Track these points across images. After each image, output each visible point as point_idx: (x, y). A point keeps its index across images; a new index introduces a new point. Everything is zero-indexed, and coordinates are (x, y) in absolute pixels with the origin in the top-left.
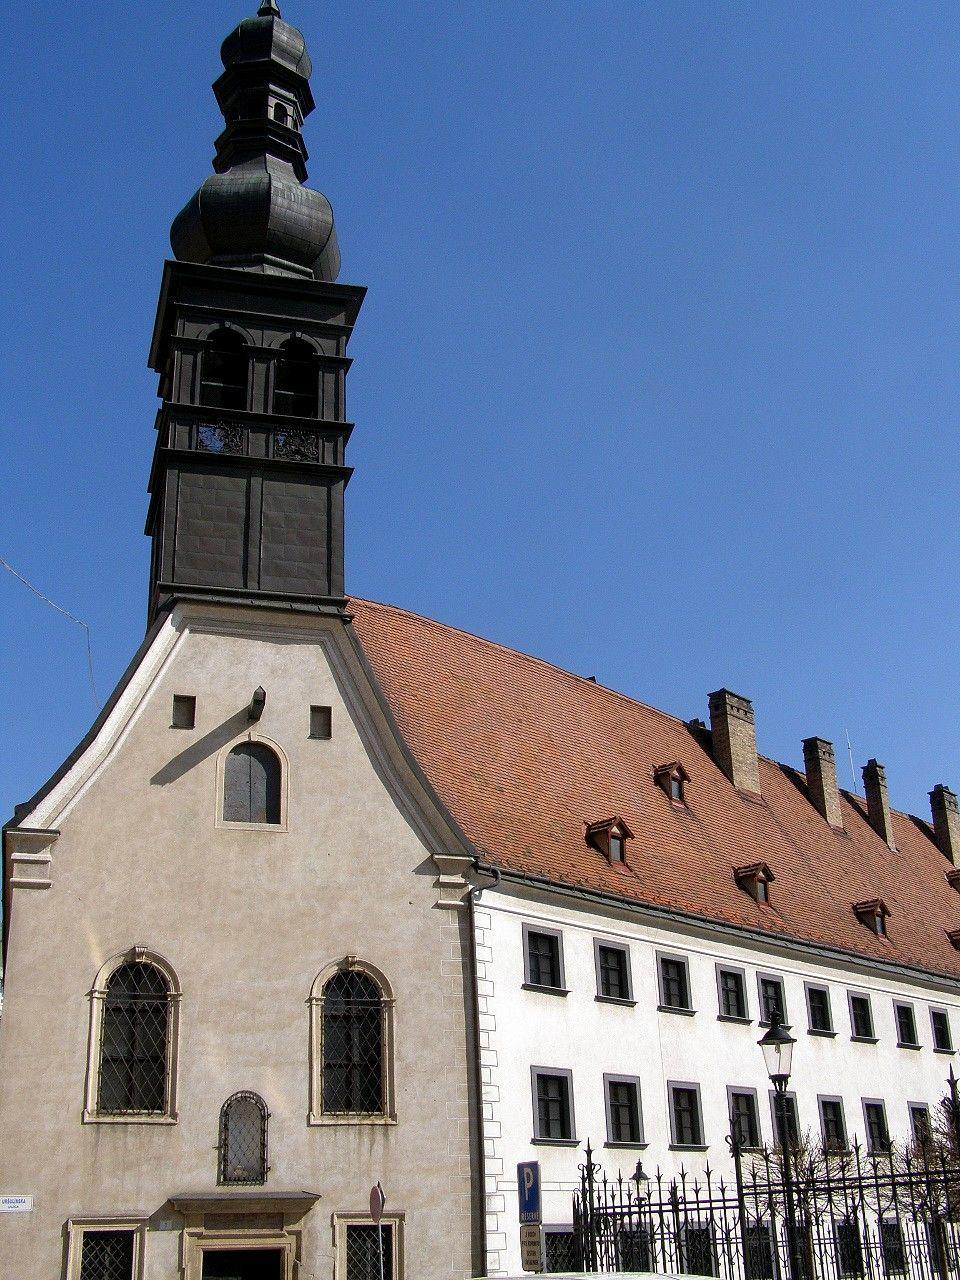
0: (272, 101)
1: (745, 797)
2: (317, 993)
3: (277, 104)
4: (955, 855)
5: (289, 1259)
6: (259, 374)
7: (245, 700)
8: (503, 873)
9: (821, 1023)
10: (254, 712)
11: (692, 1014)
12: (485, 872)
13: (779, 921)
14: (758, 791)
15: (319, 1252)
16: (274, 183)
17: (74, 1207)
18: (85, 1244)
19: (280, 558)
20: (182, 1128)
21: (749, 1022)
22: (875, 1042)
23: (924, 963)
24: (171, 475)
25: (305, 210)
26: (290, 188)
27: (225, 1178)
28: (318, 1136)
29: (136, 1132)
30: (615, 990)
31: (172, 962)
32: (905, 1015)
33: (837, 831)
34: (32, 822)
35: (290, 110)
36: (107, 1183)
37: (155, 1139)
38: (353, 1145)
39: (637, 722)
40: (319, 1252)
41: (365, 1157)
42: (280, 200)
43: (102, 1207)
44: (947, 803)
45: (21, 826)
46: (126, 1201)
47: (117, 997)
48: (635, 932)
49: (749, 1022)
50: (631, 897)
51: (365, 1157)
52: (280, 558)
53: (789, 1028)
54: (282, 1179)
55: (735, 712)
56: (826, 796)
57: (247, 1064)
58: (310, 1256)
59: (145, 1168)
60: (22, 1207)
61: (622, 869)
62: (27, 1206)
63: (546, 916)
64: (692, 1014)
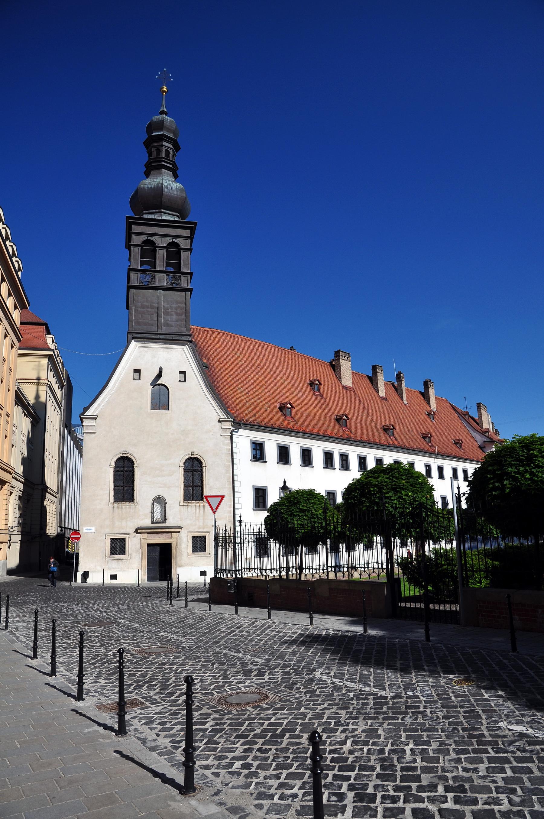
0: (164, 149)
1: (346, 388)
2: (182, 464)
3: (166, 150)
4: (431, 404)
5: (173, 546)
6: (161, 254)
7: (157, 372)
8: (242, 424)
9: (441, 475)
10: (159, 375)
11: (313, 467)
12: (238, 424)
13: (350, 434)
14: (351, 385)
15: (183, 544)
16: (164, 184)
17: (108, 531)
18: (111, 541)
19: (169, 321)
20: (139, 507)
21: (335, 469)
22: (350, 470)
23: (407, 446)
24: (131, 273)
25: (176, 193)
26: (170, 185)
27: (153, 522)
28: (182, 509)
29: (125, 508)
30: (329, 465)
31: (135, 455)
32: (455, 471)
33: (382, 398)
34: (89, 413)
35: (171, 152)
36: (117, 523)
37: (131, 510)
38: (194, 511)
39: (305, 363)
40: (183, 544)
41: (197, 515)
42: (166, 190)
43: (116, 531)
44: (429, 386)
45: (85, 414)
46: (123, 529)
47: (118, 467)
48: (293, 440)
49: (335, 469)
50: (291, 429)
51: (197, 515)
52: (169, 321)
53: (468, 486)
54: (171, 522)
55: (343, 358)
56: (379, 386)
57: (160, 487)
58: (180, 544)
59: (128, 519)
60: (91, 531)
61: (290, 419)
62: (93, 531)
63: (259, 436)
64: (313, 467)
